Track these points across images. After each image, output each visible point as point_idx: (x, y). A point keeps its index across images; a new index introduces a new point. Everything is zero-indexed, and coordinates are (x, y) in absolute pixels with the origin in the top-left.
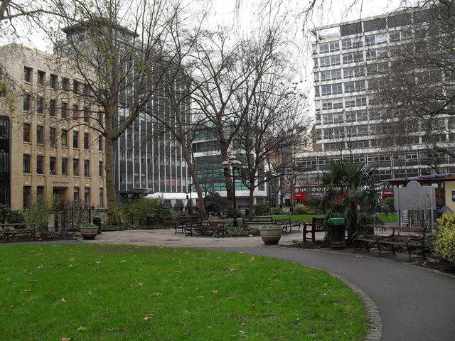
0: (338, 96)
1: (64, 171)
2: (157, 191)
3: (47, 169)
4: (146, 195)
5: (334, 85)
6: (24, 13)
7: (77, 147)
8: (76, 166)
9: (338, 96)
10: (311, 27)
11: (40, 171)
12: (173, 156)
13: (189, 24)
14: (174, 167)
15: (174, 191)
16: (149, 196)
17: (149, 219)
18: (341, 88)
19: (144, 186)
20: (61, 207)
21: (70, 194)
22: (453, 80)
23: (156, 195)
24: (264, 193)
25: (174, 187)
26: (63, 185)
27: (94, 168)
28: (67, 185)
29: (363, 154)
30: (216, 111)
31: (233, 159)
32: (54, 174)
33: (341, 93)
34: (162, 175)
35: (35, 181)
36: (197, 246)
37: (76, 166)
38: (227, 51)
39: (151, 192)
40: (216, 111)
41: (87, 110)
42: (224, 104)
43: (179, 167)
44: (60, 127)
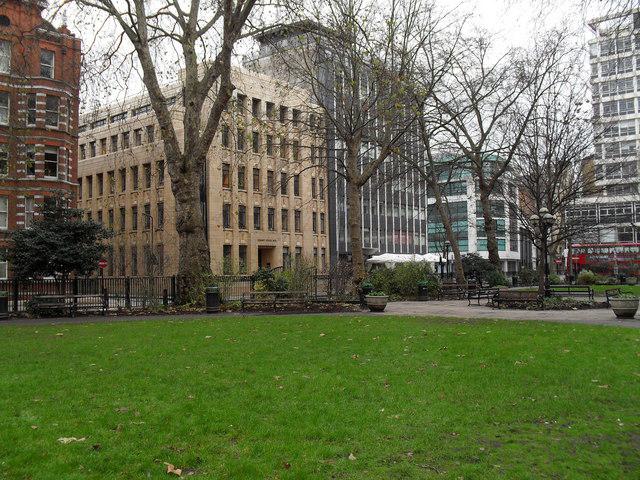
0: (628, 117)
1: (271, 226)
2: (383, 252)
3: (250, 222)
4: (370, 257)
5: (622, 102)
6: (167, 35)
7: (243, 188)
8: (285, 217)
9: (628, 117)
10: (589, 19)
11: (242, 225)
12: (404, 205)
13: (444, 28)
14: (390, 218)
15: (398, 252)
16: (375, 258)
17: (420, 287)
18: (632, 105)
19: (368, 245)
20: (264, 275)
21: (278, 259)
22: (2, 126)
23: (534, 265)
24: (517, 255)
25: (397, 246)
26: (270, 244)
27: (307, 219)
28: (274, 244)
29: (629, 203)
30: (471, 142)
31: (545, 212)
32: (258, 228)
33: (634, 112)
34: (397, 231)
35: (236, 239)
36: (260, 317)
37: (285, 217)
38: (488, 64)
39: (377, 254)
40: (471, 142)
41: (297, 145)
42: (484, 136)
43: (390, 218)
44: (251, 165)
